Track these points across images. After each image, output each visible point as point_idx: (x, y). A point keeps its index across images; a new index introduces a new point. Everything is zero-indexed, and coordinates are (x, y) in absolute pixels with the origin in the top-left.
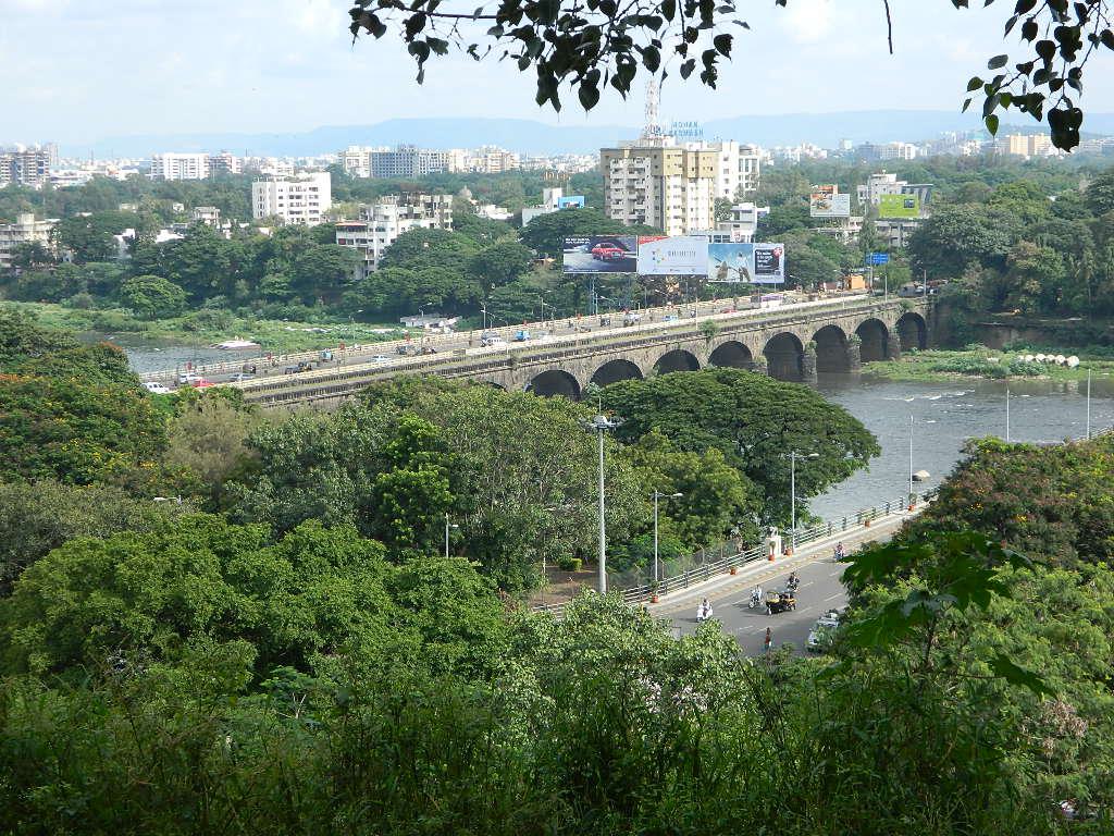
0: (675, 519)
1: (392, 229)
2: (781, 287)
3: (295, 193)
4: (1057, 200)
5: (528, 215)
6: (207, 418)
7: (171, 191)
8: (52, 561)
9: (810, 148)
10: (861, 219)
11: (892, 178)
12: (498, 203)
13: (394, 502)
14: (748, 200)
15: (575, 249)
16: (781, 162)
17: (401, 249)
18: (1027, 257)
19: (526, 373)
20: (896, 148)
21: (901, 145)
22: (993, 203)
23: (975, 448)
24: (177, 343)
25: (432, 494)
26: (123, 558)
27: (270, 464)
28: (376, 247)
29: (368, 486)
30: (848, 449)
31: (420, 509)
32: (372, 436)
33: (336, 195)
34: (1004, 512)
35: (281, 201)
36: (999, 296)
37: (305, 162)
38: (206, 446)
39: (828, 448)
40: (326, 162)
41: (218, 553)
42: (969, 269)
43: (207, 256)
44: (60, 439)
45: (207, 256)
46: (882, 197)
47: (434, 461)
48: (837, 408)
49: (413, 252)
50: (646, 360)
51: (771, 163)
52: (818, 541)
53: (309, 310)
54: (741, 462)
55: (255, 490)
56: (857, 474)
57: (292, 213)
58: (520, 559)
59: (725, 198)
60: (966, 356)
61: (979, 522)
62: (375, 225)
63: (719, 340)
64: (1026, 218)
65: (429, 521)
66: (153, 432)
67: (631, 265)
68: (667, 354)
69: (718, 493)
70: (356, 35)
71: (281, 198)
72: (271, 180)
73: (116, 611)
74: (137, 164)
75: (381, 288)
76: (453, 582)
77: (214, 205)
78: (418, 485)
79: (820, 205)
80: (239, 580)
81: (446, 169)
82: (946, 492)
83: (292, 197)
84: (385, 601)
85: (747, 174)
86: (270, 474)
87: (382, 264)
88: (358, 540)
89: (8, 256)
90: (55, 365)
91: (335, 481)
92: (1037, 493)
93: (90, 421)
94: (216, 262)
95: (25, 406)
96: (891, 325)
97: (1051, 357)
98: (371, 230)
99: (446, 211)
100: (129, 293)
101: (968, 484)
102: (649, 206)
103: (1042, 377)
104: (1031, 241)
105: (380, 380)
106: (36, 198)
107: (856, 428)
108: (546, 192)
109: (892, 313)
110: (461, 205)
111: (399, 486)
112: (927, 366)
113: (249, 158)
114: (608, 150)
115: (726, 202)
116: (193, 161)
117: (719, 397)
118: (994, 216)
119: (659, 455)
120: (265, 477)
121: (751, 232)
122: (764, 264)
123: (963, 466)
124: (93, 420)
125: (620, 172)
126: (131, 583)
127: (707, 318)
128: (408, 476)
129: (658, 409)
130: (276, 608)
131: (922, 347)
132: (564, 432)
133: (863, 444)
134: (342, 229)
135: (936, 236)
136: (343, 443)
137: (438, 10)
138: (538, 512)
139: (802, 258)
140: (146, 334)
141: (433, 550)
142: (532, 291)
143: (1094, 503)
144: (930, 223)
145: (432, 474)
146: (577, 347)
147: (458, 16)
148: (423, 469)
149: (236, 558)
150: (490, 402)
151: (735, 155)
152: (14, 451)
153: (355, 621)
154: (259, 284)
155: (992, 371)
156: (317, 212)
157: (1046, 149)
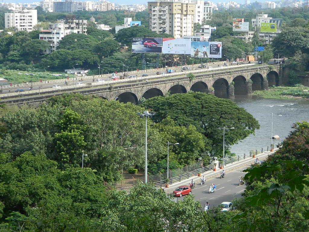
0: (176, 153)
1: (62, 33)
2: (221, 60)
3: (22, 18)
5: (118, 28)
10: (253, 32)
11: (266, 16)
12: (106, 23)
13: (61, 145)
15: (137, 43)
16: (221, 8)
17: (66, 42)
20: (268, 4)
21: (270, 3)
23: (298, 126)
27: (10, 128)
28: (56, 40)
29: (51, 138)
30: (246, 126)
32: (53, 118)
33: (39, 19)
35: (17, 21)
37: (26, 5)
39: (238, 125)
46: (262, 23)
47: (78, 129)
48: (242, 109)
49: (70, 43)
50: (165, 89)
51: (217, 9)
52: (234, 163)
53: (28, 66)
55: (4, 139)
57: (21, 26)
59: (198, 23)
60: (295, 89)
62: (55, 31)
63: (195, 81)
65: (75, 153)
67: (160, 50)
71: (17, 20)
72: (13, 12)
75: (57, 58)
76: (85, 178)
78: (71, 138)
83: (21, 20)
84: (57, 186)
85: (207, 13)
86: (10, 133)
87: (58, 48)
91: (38, 136)
96: (265, 76)
98: (54, 34)
99: (84, 26)
102: (167, 26)
105: (56, 95)
107: (250, 117)
108: (125, 19)
109: (265, 71)
110: (90, 24)
111: (63, 138)
112: (279, 93)
113: (3, 3)
114: (151, 3)
115: (198, 25)
117: (194, 104)
120: (9, 134)
122: (214, 50)
123: (293, 134)
125: (156, 12)
127: (190, 72)
128: (67, 135)
130: (13, 188)
131: (277, 85)
133: (253, 124)
134: (41, 33)
135: (283, 40)
136: (41, 120)
138: (121, 149)
139: (229, 48)
142: (119, 59)
144: (281, 35)
145: (77, 134)
146: (137, 83)
148: (74, 132)
150: (101, 105)
151: (202, 6)
153: (44, 193)
154: (7, 55)
155: (305, 95)
156: (31, 26)
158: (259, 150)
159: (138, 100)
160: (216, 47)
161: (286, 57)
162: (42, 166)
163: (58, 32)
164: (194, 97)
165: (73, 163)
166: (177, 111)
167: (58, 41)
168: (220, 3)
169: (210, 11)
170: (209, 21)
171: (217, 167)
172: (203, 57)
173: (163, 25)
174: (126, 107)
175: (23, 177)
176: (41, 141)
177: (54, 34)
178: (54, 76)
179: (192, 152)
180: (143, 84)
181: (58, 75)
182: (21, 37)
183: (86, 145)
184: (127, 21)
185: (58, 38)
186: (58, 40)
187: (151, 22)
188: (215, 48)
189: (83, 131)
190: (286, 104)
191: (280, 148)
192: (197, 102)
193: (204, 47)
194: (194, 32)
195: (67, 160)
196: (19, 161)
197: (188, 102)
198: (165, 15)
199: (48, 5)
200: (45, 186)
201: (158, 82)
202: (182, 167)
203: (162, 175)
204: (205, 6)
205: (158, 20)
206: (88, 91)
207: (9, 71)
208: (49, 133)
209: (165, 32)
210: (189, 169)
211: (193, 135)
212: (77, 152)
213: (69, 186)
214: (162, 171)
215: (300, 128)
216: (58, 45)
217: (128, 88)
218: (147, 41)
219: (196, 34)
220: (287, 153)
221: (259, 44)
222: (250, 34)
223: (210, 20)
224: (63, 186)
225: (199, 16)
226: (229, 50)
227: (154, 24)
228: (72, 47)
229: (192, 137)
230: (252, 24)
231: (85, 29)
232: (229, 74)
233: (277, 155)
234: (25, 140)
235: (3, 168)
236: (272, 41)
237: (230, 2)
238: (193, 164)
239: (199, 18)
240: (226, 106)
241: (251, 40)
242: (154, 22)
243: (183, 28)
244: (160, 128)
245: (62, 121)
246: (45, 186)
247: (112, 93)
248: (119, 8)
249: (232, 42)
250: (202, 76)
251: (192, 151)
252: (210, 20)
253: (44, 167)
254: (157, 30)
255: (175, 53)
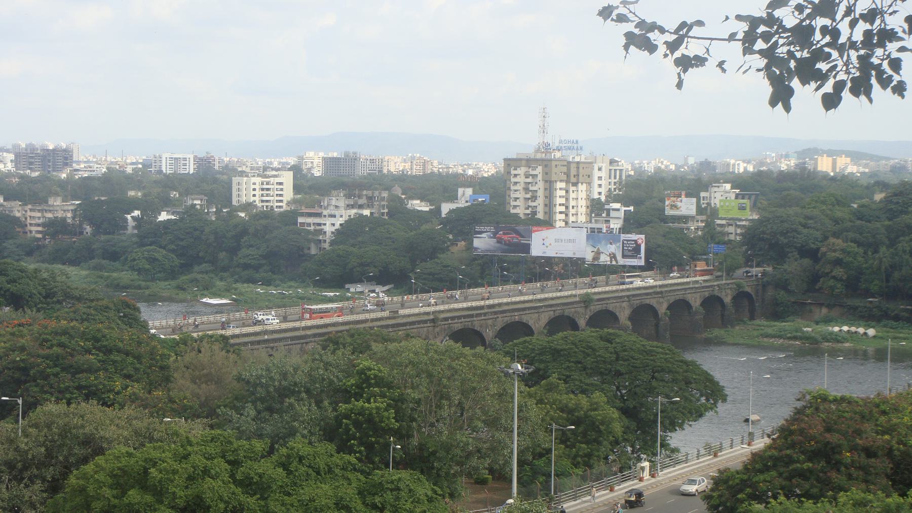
0: (567, 446)
2: (641, 269)
3: (265, 186)
4: (858, 206)
5: (446, 208)
6: (204, 357)
7: (174, 181)
8: (97, 466)
9: (662, 163)
10: (704, 218)
11: (728, 186)
13: (351, 427)
14: (616, 200)
15: (484, 235)
16: (639, 171)
17: (348, 231)
18: (835, 251)
19: (445, 330)
20: (728, 165)
21: (732, 162)
22: (809, 208)
23: (808, 397)
24: (171, 300)
25: (382, 422)
26: (155, 464)
28: (328, 229)
29: (331, 414)
30: (702, 395)
31: (371, 433)
33: (297, 188)
34: (833, 449)
35: (254, 193)
36: (813, 280)
38: (203, 380)
39: (686, 394)
40: (288, 164)
41: (229, 462)
42: (789, 258)
43: (197, 233)
44: (90, 370)
45: (197, 233)
46: (721, 201)
47: (383, 396)
48: (693, 363)
50: (539, 322)
51: (632, 173)
52: (678, 467)
54: (618, 403)
55: (241, 415)
56: (709, 414)
57: (262, 201)
58: (447, 474)
60: (786, 325)
61: (813, 456)
63: (595, 308)
64: (836, 221)
66: (162, 368)
67: (527, 248)
68: (554, 318)
69: (601, 427)
70: (627, 53)
71: (254, 190)
72: (247, 176)
73: (148, 506)
74: (141, 161)
76: (410, 490)
77: (202, 194)
78: (371, 414)
79: (673, 207)
80: (247, 485)
81: (380, 171)
82: (785, 432)
83: (263, 189)
85: (616, 181)
86: (254, 403)
87: (332, 243)
88: (336, 455)
89: (40, 229)
90: (84, 313)
91: (305, 409)
92: (859, 435)
93: (112, 357)
94: (203, 237)
95: (61, 345)
96: (728, 300)
97: (853, 329)
99: (383, 203)
100: (134, 260)
101: (803, 425)
102: (540, 203)
103: (847, 345)
104: (838, 238)
105: (337, 332)
106: (62, 184)
108: (460, 191)
109: (729, 291)
110: (394, 199)
112: (756, 333)
113: (228, 159)
114: (510, 160)
116: (185, 159)
117: (601, 352)
118: (810, 218)
119: (556, 396)
120: (249, 405)
121: (619, 226)
122: (629, 251)
123: (799, 412)
124: (115, 357)
125: (518, 177)
126: (160, 484)
127: (585, 291)
129: (554, 360)
131: (752, 318)
132: (484, 375)
134: (302, 215)
135: (764, 233)
137: (691, 34)
138: (462, 437)
139: (659, 246)
140: (147, 292)
141: (380, 465)
143: (905, 445)
144: (760, 222)
145: (382, 406)
147: (712, 39)
148: (375, 402)
149: (243, 466)
150: (427, 351)
151: (605, 166)
152: (53, 380)
155: (807, 338)
156: (281, 201)
157: (846, 167)
158: (726, 444)
159: (487, 343)
160: (635, 245)
161: (768, 265)
162: (328, 466)
163: (333, 212)
164: (601, 338)
165: (373, 463)
166: (567, 364)
167: (334, 231)
168: (636, 162)
169: (620, 176)
170: (618, 195)
171: (646, 475)
172: (609, 263)
173: (532, 201)
174: (474, 355)
175: (292, 486)
176: (311, 419)
177: (325, 216)
178: (326, 296)
179: (598, 444)
180: (495, 313)
181: (332, 294)
182: (263, 222)
183: (399, 428)
184: (464, 194)
185: (333, 225)
186: (333, 229)
187: (509, 196)
188: (632, 246)
189: (393, 400)
190: (770, 355)
191: (773, 439)
192: (607, 349)
193: (611, 244)
194: (591, 215)
195: (362, 456)
196: (284, 456)
197: (590, 347)
198: (536, 183)
199: (312, 163)
200: (335, 504)
201: (524, 309)
202: (579, 471)
203: (541, 488)
204: (611, 168)
205: (523, 193)
206: (393, 326)
207: (239, 285)
208: (327, 404)
209: (536, 215)
210: (592, 478)
211: (601, 412)
212: (381, 440)
213: (380, 506)
214: (541, 480)
215: (812, 401)
216: (334, 238)
217: (469, 320)
218: (501, 232)
219: (595, 220)
220: (788, 448)
221: (717, 240)
222: (698, 221)
223: (621, 193)
224: (368, 505)
225: (600, 186)
226: (659, 250)
227: (516, 199)
228: (359, 242)
229: (599, 415)
230: (702, 202)
231: (384, 209)
232: (660, 296)
233: (770, 454)
234: (281, 417)
235: (255, 470)
236: (741, 234)
237: (655, 160)
238: (601, 467)
239: (600, 190)
240: (662, 356)
241: (700, 233)
242: (516, 196)
243: (571, 207)
244: (538, 398)
245: (353, 381)
246: (335, 504)
247: (437, 330)
248: (445, 170)
249: (664, 236)
250: (608, 299)
251: (599, 443)
252: (621, 193)
253: (331, 468)
254: (521, 211)
255: (555, 255)
